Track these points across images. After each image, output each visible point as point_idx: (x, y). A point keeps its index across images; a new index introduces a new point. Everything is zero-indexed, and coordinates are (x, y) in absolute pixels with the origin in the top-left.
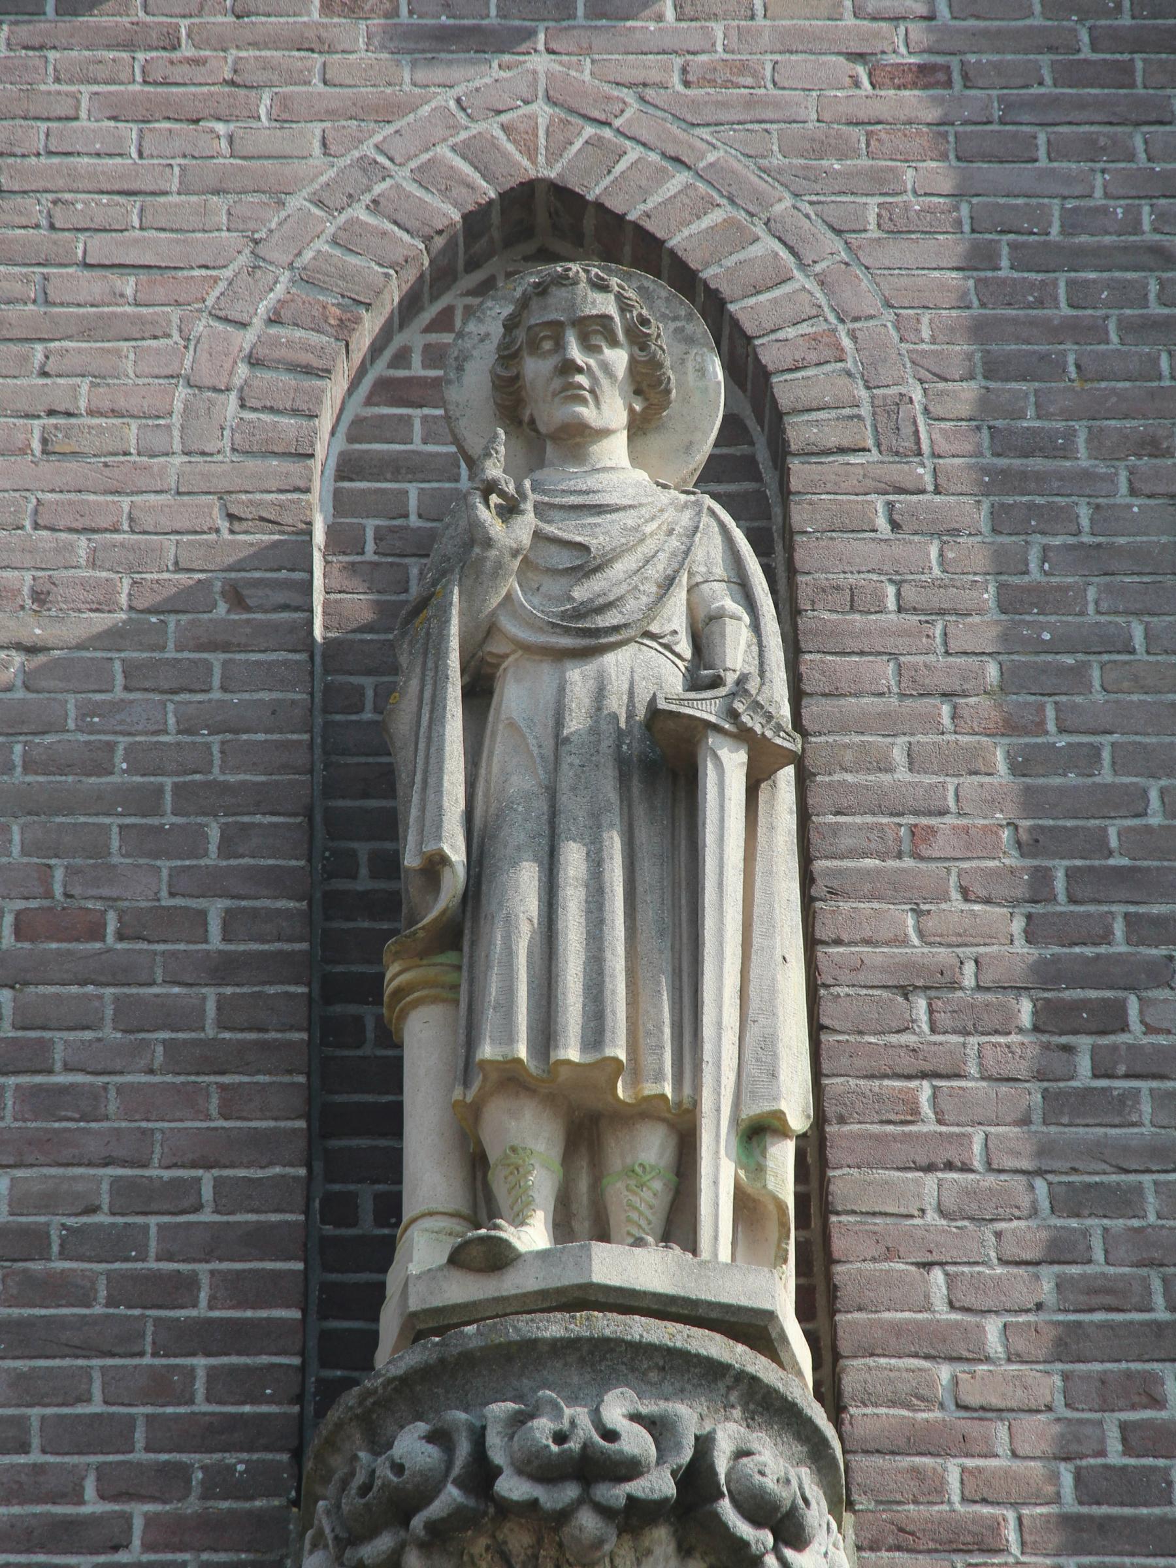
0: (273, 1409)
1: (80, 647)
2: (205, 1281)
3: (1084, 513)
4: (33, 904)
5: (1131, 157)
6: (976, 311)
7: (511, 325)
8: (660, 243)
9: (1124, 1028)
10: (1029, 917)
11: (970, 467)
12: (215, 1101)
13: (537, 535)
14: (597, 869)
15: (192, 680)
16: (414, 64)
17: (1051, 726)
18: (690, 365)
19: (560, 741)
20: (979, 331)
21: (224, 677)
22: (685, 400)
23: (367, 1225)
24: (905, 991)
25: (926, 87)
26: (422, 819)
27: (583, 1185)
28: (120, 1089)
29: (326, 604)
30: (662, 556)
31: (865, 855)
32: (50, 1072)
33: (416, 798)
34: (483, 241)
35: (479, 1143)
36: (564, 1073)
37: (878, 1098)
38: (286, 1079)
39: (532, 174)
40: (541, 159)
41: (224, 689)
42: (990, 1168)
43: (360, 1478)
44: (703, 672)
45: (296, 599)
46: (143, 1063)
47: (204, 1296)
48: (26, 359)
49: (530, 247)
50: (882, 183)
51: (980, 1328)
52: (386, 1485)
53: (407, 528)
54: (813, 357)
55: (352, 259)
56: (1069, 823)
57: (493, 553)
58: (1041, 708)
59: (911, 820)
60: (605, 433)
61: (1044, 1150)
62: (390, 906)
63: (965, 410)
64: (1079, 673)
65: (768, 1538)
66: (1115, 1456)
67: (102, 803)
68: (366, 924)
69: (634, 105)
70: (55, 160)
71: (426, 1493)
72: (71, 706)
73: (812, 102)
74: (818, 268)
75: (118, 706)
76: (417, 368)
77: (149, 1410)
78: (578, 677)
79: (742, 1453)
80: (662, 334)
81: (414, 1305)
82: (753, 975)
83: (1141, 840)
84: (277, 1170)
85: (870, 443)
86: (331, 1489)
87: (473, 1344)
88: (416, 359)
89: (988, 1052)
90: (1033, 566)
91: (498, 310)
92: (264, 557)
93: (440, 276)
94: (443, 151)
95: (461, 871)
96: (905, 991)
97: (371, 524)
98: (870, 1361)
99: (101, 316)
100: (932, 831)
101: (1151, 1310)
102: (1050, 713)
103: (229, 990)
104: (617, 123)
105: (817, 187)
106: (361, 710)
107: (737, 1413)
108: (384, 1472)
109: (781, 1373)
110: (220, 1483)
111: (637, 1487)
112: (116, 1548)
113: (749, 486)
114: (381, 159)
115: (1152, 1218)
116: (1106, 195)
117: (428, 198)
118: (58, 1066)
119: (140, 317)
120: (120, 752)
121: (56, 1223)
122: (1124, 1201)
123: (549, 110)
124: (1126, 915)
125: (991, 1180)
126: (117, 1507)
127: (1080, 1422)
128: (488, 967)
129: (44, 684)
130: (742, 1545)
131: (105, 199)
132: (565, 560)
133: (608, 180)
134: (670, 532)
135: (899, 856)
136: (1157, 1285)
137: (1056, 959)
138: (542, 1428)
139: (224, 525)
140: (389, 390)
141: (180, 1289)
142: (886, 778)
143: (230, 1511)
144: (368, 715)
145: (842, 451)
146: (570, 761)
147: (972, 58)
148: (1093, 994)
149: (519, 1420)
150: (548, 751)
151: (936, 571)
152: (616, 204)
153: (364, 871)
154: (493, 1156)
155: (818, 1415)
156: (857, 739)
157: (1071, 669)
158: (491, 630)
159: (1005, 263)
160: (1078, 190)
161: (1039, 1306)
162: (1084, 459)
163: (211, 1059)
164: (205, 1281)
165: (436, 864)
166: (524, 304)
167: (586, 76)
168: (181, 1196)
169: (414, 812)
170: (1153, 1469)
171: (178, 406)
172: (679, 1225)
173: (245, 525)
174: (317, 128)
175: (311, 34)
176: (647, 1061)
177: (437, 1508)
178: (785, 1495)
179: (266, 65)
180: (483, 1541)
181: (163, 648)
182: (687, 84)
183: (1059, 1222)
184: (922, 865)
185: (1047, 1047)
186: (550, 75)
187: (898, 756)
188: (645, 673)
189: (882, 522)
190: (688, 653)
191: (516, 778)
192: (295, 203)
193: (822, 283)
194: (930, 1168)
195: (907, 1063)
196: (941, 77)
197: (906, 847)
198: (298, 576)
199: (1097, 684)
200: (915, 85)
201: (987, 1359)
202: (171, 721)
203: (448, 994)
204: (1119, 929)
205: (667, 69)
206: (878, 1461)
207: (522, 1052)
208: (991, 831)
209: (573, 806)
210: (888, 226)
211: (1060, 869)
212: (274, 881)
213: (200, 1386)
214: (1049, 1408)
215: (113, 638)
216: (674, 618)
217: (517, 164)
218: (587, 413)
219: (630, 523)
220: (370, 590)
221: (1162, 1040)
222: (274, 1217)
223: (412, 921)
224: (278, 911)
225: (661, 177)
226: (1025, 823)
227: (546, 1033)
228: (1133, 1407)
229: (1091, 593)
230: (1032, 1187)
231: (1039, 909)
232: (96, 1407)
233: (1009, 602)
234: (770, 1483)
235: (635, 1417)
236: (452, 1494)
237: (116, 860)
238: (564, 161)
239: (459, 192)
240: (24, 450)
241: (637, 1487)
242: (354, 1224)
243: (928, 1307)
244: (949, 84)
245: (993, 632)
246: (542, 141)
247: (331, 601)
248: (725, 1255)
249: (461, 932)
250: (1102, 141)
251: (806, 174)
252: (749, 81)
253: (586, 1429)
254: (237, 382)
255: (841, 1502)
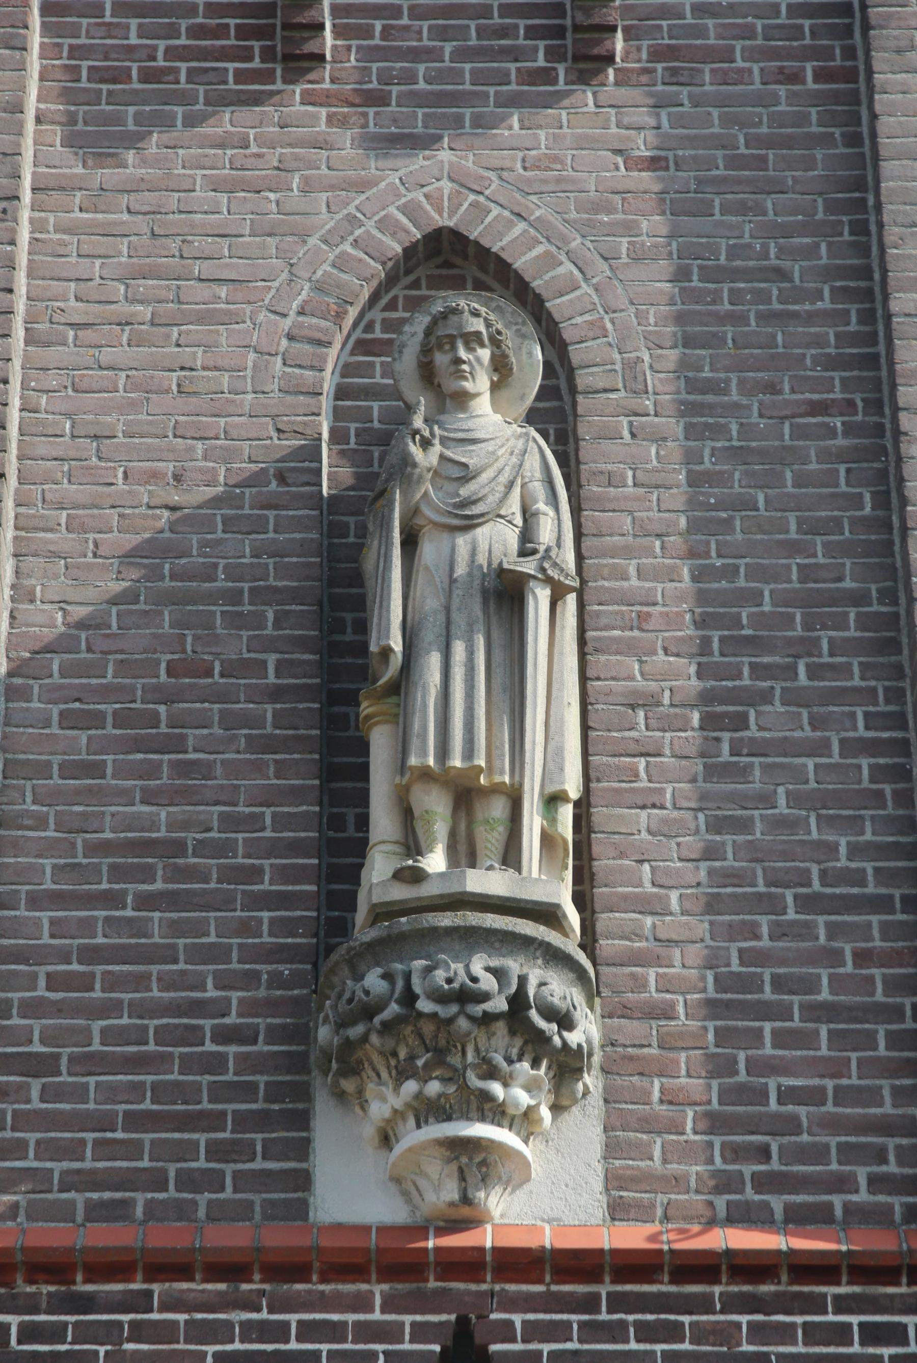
0: (303, 940)
1: (199, 507)
2: (267, 869)
3: (734, 428)
4: (176, 657)
5: (765, 214)
6: (679, 307)
7: (428, 332)
8: (509, 265)
9: (747, 728)
10: (699, 664)
11: (674, 400)
12: (272, 769)
13: (442, 457)
14: (471, 654)
15: (260, 526)
16: (377, 157)
17: (713, 554)
18: (524, 351)
19: (452, 581)
20: (680, 319)
21: (275, 525)
22: (521, 369)
23: (351, 832)
24: (633, 707)
25: (654, 170)
26: (379, 624)
27: (463, 826)
28: (223, 762)
29: (329, 474)
30: (507, 469)
31: (613, 628)
32: (186, 752)
33: (376, 612)
34: (414, 260)
35: (409, 804)
36: (453, 772)
37: (618, 768)
38: (309, 756)
39: (441, 224)
40: (445, 215)
41: (275, 532)
42: (675, 807)
43: (347, 995)
44: (527, 536)
45: (313, 479)
46: (234, 748)
47: (267, 878)
48: (168, 336)
49: (439, 260)
50: (630, 229)
51: (668, 896)
52: (360, 1000)
53: (371, 429)
54: (591, 334)
55: (343, 275)
56: (722, 610)
57: (418, 470)
58: (708, 543)
59: (638, 608)
60: (477, 395)
61: (703, 797)
62: (365, 674)
63: (671, 366)
64: (729, 521)
65: (555, 1027)
66: (735, 967)
67: (211, 598)
68: (350, 660)
69: (496, 182)
70: (183, 216)
71: (380, 1006)
72: (194, 542)
73: (593, 181)
74: (594, 281)
75: (219, 542)
76: (378, 334)
77: (239, 940)
78: (462, 542)
79: (542, 984)
80: (509, 339)
81: (375, 900)
82: (552, 713)
83: (759, 620)
84: (304, 808)
85: (620, 386)
86: (333, 995)
87: (405, 928)
88: (378, 327)
89: (676, 742)
90: (706, 459)
91: (422, 321)
92: (297, 454)
93: (391, 280)
94: (392, 210)
95: (400, 656)
96: (633, 707)
97: (353, 426)
98: (611, 915)
99: (208, 310)
100: (649, 615)
101: (755, 886)
102: (713, 546)
103: (278, 706)
104: (487, 192)
105: (595, 232)
106: (347, 536)
107: (540, 961)
108: (360, 994)
109: (563, 939)
110: (276, 981)
111: (488, 1006)
112: (223, 1016)
113: (555, 404)
114: (359, 215)
115: (758, 835)
116: (752, 237)
117: (384, 238)
118: (190, 749)
119: (229, 311)
120: (221, 568)
121: (191, 837)
122: (745, 826)
123: (450, 185)
124: (750, 663)
125: (676, 814)
126: (223, 994)
127: (718, 948)
128: (414, 713)
129: (180, 529)
130: (542, 1032)
131: (210, 239)
132: (456, 473)
133: (481, 227)
134: (512, 453)
135: (631, 629)
136: (760, 873)
137: (713, 688)
138: (440, 975)
139: (274, 435)
140: (363, 347)
141: (254, 874)
142: (625, 584)
143: (281, 996)
144: (351, 539)
145: (606, 391)
146: (457, 593)
147: (680, 153)
148: (731, 708)
149: (429, 970)
150: (446, 586)
151: (655, 462)
152: (485, 242)
153: (349, 630)
154: (417, 813)
155: (581, 957)
156: (611, 561)
157: (725, 520)
158: (416, 511)
159: (695, 278)
160: (736, 233)
161: (698, 884)
162: (735, 396)
163: (269, 745)
164: (267, 869)
165: (387, 651)
166: (435, 322)
167: (470, 164)
168: (253, 822)
169: (375, 620)
170: (755, 974)
171: (250, 364)
172: (511, 856)
173: (286, 435)
174: (324, 196)
175: (320, 138)
176: (496, 763)
177: (386, 1015)
178: (563, 1006)
179: (297, 158)
180: (410, 1029)
181: (242, 508)
182: (525, 169)
183: (710, 837)
184: (643, 634)
185: (706, 739)
186: (451, 164)
187: (632, 571)
188: (497, 540)
189: (626, 433)
190: (520, 524)
191: (430, 603)
192: (313, 241)
193: (596, 290)
194: (643, 807)
195: (633, 748)
196: (663, 164)
197: (635, 624)
198: (314, 465)
199: (738, 529)
200: (648, 169)
201: (671, 914)
202: (248, 550)
203: (393, 719)
204: (746, 671)
205: (514, 159)
206: (613, 969)
207: (431, 762)
208: (680, 615)
209: (459, 619)
210: (633, 255)
211: (716, 636)
212: (301, 643)
213: (265, 928)
214: (702, 940)
215: (216, 502)
216: (514, 507)
217: (432, 218)
218: (468, 385)
219: (491, 449)
220: (352, 466)
221: (767, 735)
222: (303, 834)
223: (375, 681)
224: (304, 661)
225: (510, 225)
226: (698, 610)
227: (443, 752)
228: (745, 940)
229: (737, 476)
230: (696, 818)
231: (704, 659)
232: (212, 939)
233: (694, 480)
234: (556, 1001)
235: (488, 969)
236: (394, 1008)
237: (219, 631)
238: (458, 216)
239: (401, 235)
240: (168, 391)
241: (488, 1006)
242: (344, 831)
243: (641, 885)
244: (667, 169)
245: (683, 499)
246: (446, 204)
247: (332, 474)
248: (535, 874)
249: (401, 687)
250: (750, 204)
251: (590, 224)
252: (559, 167)
253: (462, 977)
254: (282, 349)
255: (592, 993)
